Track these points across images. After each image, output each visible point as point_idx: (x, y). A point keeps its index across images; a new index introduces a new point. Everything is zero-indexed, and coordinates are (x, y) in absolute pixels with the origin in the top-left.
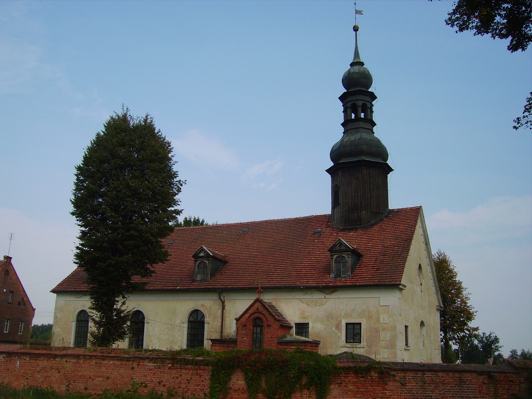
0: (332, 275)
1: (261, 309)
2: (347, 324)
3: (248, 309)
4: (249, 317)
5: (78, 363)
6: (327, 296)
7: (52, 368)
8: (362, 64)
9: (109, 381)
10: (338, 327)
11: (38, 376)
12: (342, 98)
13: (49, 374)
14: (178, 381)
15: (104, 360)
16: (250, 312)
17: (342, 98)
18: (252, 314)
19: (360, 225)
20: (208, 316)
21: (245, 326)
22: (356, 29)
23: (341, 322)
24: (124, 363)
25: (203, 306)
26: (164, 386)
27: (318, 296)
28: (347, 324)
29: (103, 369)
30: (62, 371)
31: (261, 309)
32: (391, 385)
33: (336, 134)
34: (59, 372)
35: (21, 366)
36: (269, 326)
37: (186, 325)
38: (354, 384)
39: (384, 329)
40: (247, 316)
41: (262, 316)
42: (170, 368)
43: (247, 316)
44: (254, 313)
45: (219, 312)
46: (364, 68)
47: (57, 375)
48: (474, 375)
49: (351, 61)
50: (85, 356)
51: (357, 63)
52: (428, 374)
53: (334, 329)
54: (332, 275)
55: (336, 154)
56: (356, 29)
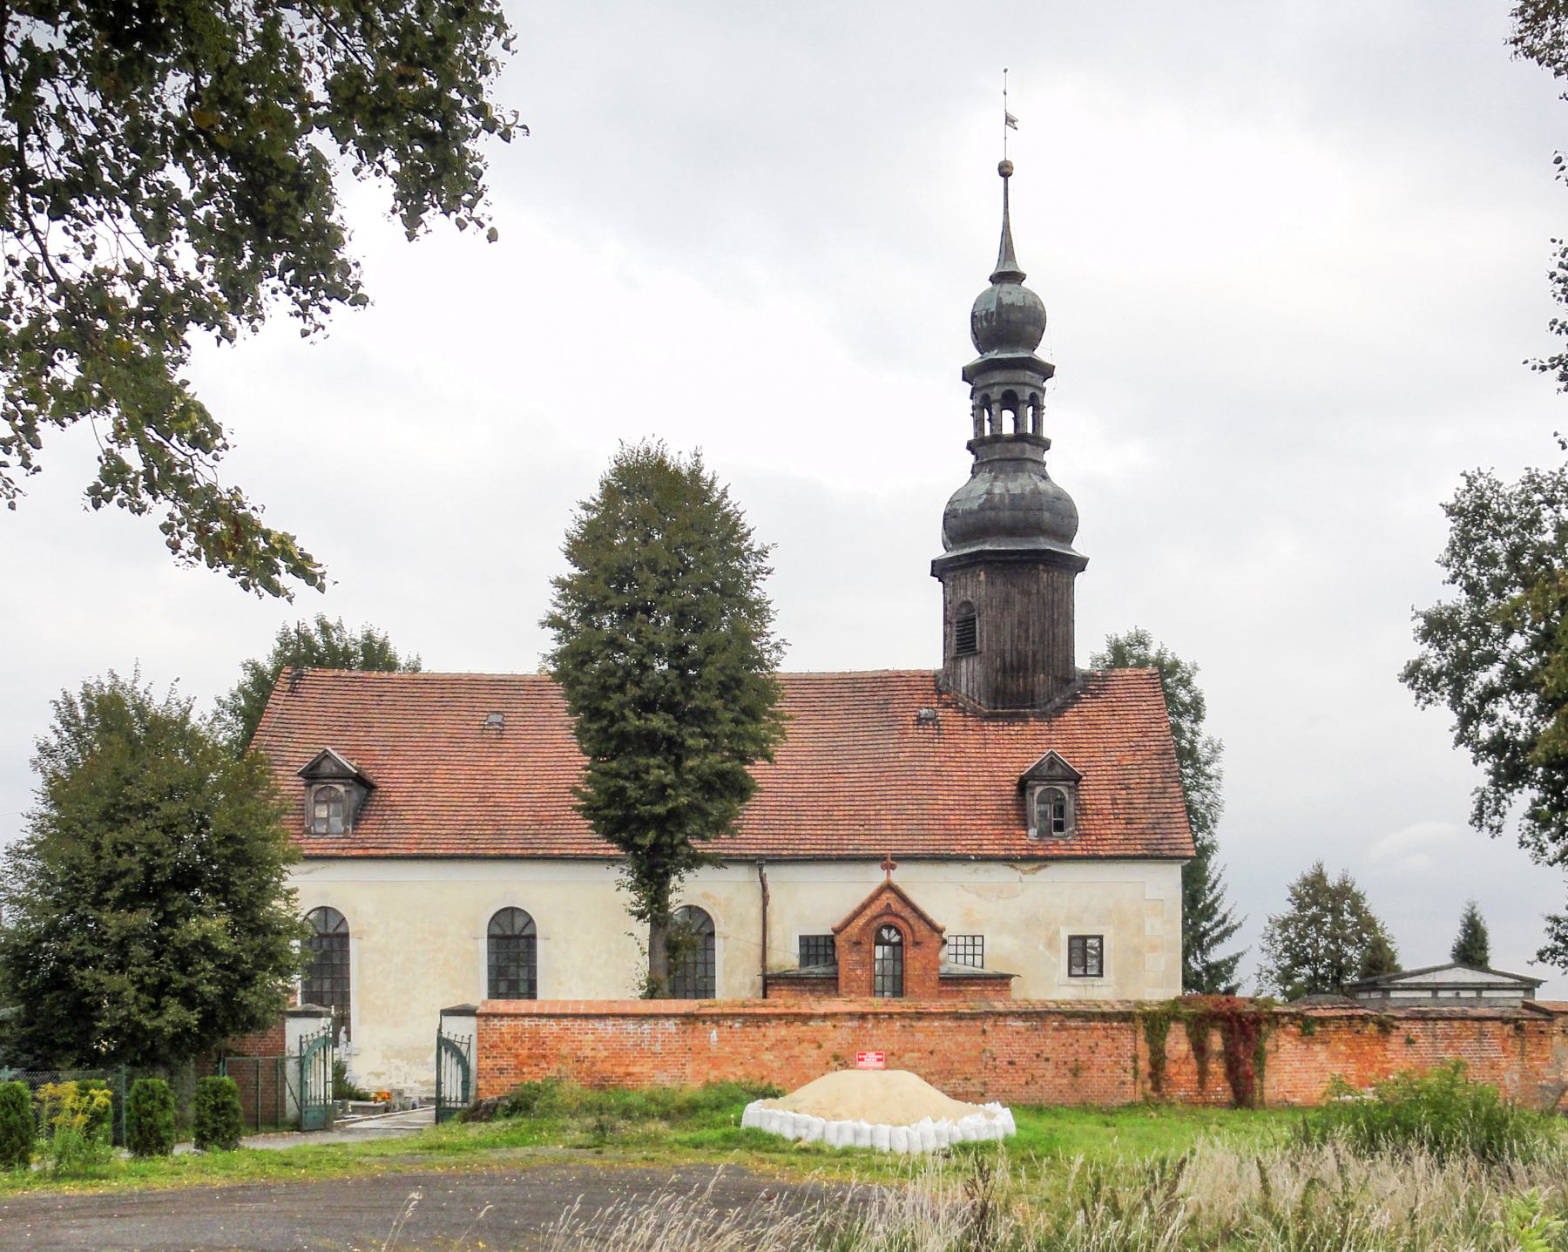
0: (1033, 832)
1: (897, 906)
2: (1072, 938)
3: (864, 907)
4: (868, 924)
5: (861, 1027)
6: (1026, 878)
7: (800, 1041)
8: (1017, 277)
9: (935, 1058)
10: (1051, 944)
11: (768, 1057)
12: (969, 375)
13: (796, 1051)
14: (1071, 1050)
15: (920, 1019)
16: (869, 913)
17: (969, 375)
18: (875, 918)
19: (1033, 707)
20: (722, 920)
21: (858, 943)
22: (1005, 171)
23: (1057, 932)
24: (963, 1023)
25: (706, 896)
26: (1047, 1060)
27: (1001, 875)
28: (1072, 938)
29: (920, 1036)
30: (826, 1045)
31: (897, 906)
32: (1395, 1042)
33: (950, 471)
34: (820, 1047)
35: (721, 1040)
36: (917, 944)
37: (483, 945)
38: (1346, 1043)
39: (1154, 948)
40: (861, 921)
41: (901, 923)
42: (1056, 1029)
43: (861, 921)
44: (880, 916)
45: (755, 912)
46: (1028, 292)
47: (814, 1053)
48: (1498, 1024)
49: (992, 270)
50: (876, 1015)
51: (1007, 276)
52: (1441, 1024)
53: (1041, 948)
54: (1033, 832)
55: (961, 525)
56: (1005, 171)
